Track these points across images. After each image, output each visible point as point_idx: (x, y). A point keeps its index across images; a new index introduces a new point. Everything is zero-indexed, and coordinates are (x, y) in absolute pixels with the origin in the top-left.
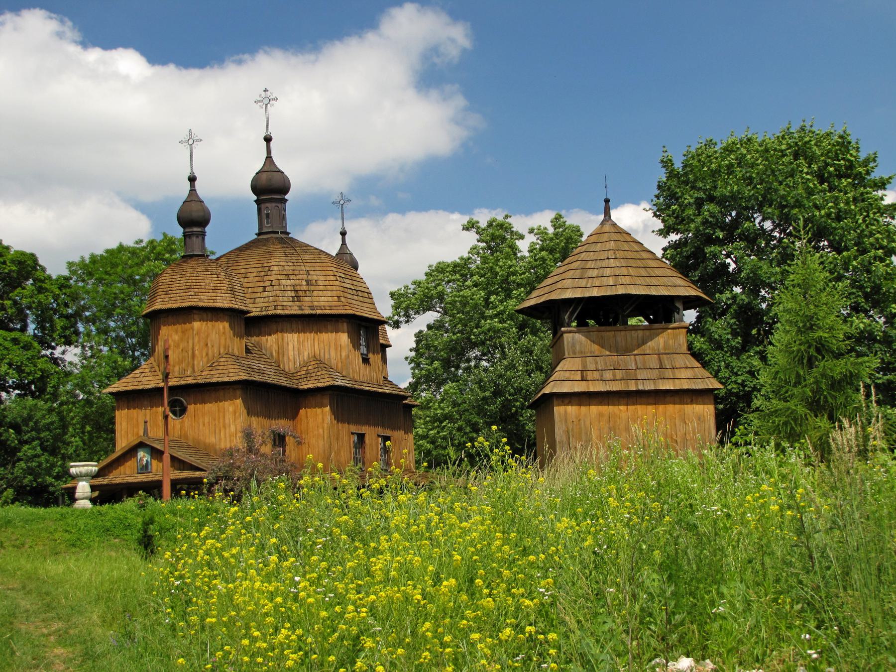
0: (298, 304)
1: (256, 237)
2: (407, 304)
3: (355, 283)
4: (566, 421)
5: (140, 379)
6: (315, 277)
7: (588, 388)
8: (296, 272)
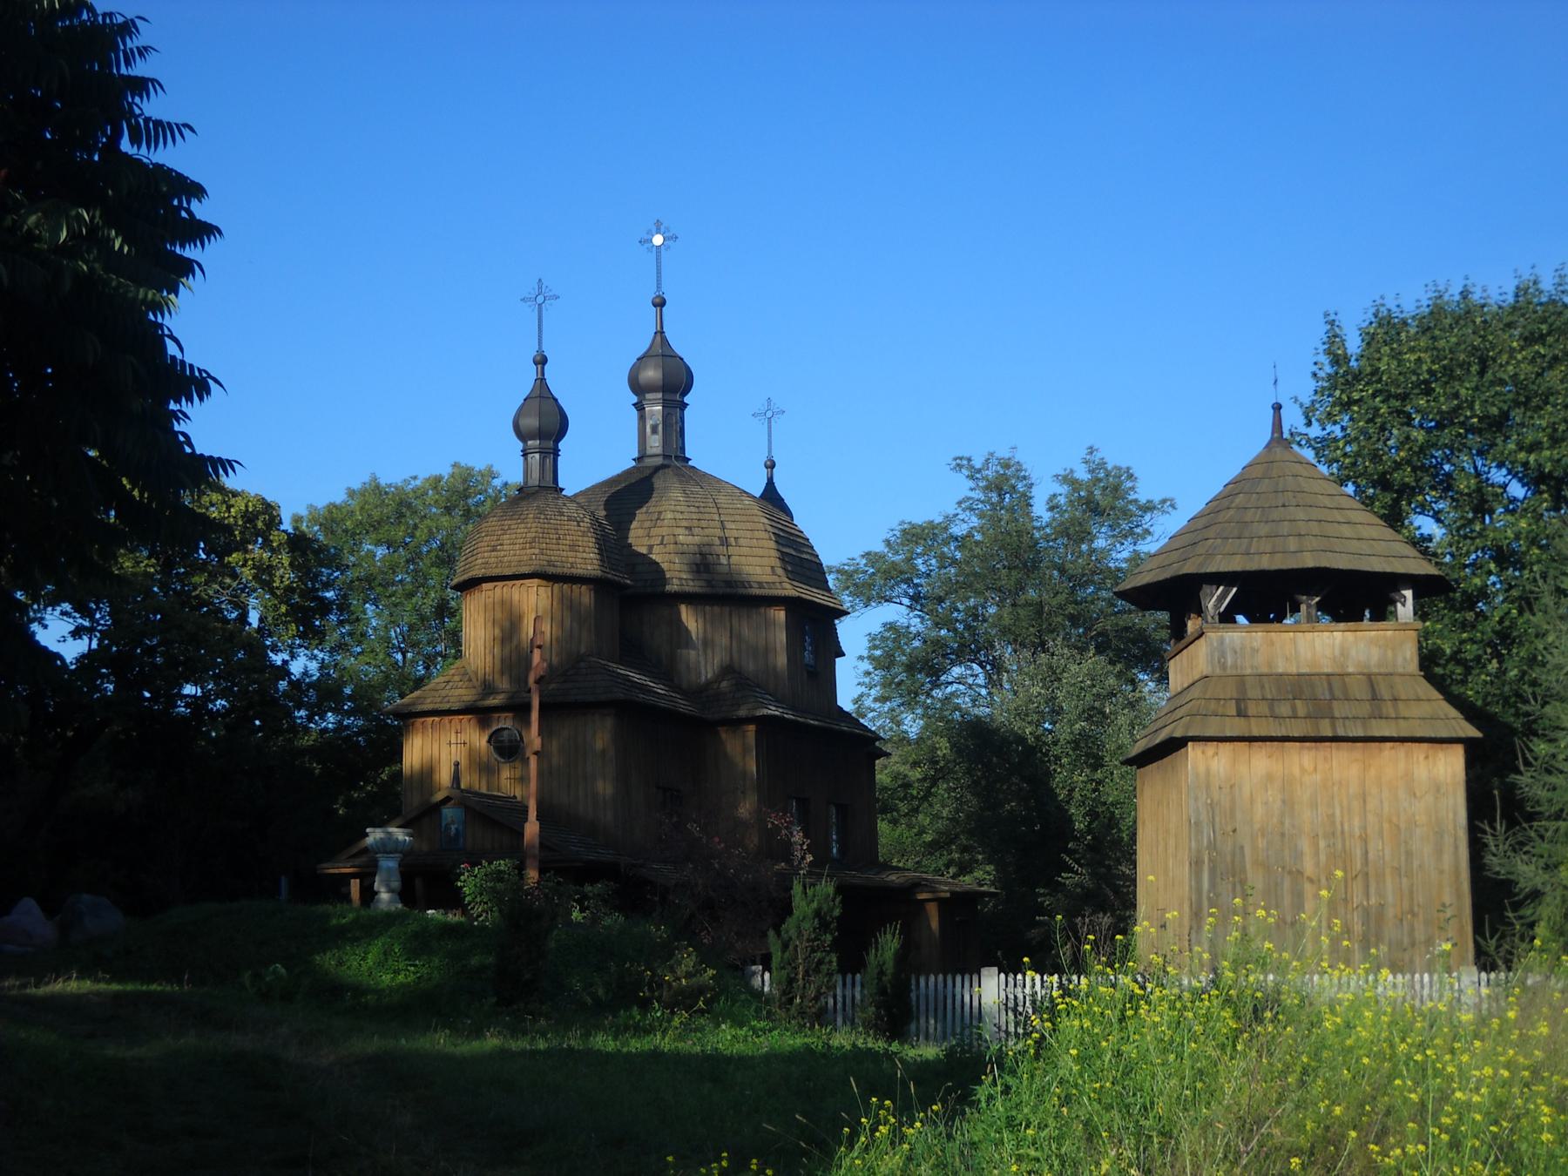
2: (879, 579)
4: (1208, 787)
5: (444, 693)
6: (735, 534)
8: (703, 523)
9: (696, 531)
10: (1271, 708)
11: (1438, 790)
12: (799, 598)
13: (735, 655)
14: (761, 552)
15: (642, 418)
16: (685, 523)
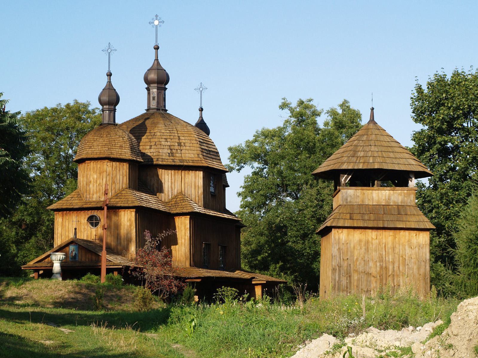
0: (172, 158)
1: (145, 112)
2: (240, 156)
3: (209, 146)
5: (71, 202)
7: (354, 224)
8: (172, 137)
9: (169, 140)
10: (362, 217)
11: (420, 246)
12: (208, 167)
13: (183, 190)
14: (193, 148)
15: (149, 94)
16: (164, 137)
